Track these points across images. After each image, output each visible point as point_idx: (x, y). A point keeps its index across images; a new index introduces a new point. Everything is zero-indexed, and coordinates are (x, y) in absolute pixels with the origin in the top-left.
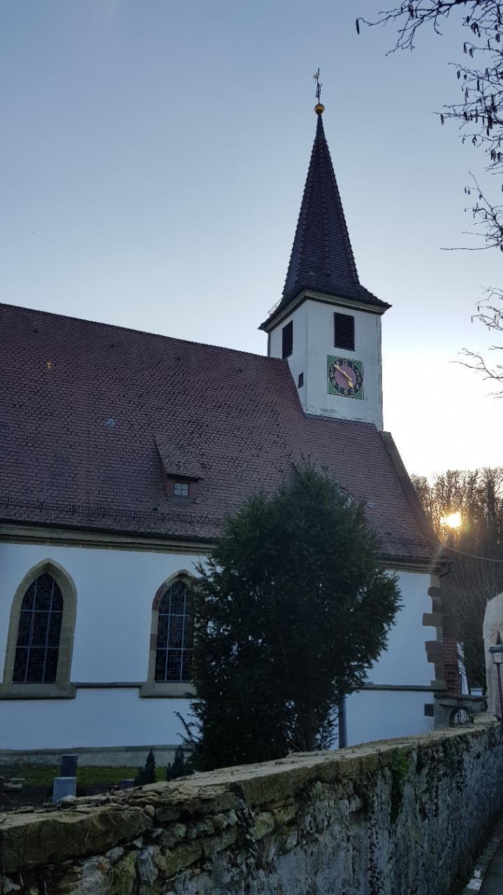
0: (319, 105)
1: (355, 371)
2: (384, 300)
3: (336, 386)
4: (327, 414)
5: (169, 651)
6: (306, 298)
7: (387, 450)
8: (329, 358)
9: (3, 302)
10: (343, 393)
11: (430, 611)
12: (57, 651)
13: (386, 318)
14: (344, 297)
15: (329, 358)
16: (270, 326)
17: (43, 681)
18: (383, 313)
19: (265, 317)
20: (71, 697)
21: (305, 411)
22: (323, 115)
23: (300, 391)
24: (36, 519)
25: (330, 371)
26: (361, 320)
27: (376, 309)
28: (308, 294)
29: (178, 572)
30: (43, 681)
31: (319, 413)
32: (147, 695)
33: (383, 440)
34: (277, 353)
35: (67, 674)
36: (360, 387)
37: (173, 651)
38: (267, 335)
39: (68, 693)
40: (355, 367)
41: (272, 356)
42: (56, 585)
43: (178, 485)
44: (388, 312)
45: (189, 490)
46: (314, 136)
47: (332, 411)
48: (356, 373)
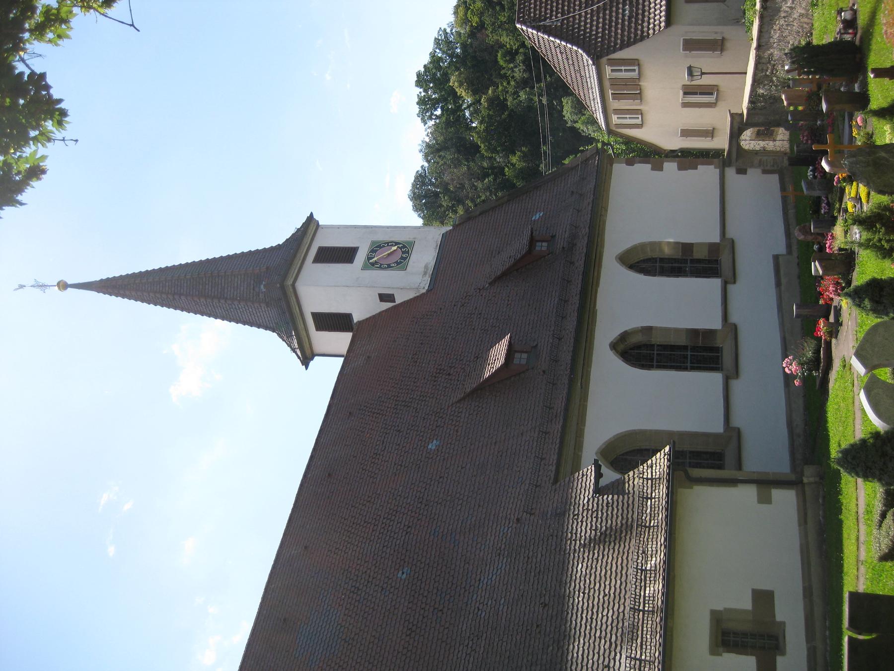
0: (58, 284)
1: (382, 247)
2: (299, 223)
3: (398, 263)
4: (430, 272)
5: (691, 363)
6: (293, 285)
7: (476, 217)
8: (365, 267)
9: (238, 668)
10: (407, 258)
11: (649, 166)
12: (691, 452)
13: (322, 219)
14: (295, 256)
15: (365, 267)
16: (308, 352)
17: (721, 462)
18: (318, 221)
19: (294, 360)
20: (732, 242)
21: (424, 291)
22: (69, 282)
23: (399, 300)
24: (555, 457)
25: (380, 268)
26: (323, 241)
27: (312, 228)
28: (289, 282)
29: (612, 350)
30: (721, 462)
31: (427, 279)
32: (736, 373)
33: (463, 223)
34: (342, 340)
35: (716, 436)
36: (400, 244)
37: (691, 360)
38: (316, 358)
39: (733, 330)
40: (376, 247)
41: (344, 350)
42: (623, 455)
43: (516, 361)
44: (315, 217)
45: (522, 352)
46: (93, 294)
47: (426, 267)
48: (384, 246)
